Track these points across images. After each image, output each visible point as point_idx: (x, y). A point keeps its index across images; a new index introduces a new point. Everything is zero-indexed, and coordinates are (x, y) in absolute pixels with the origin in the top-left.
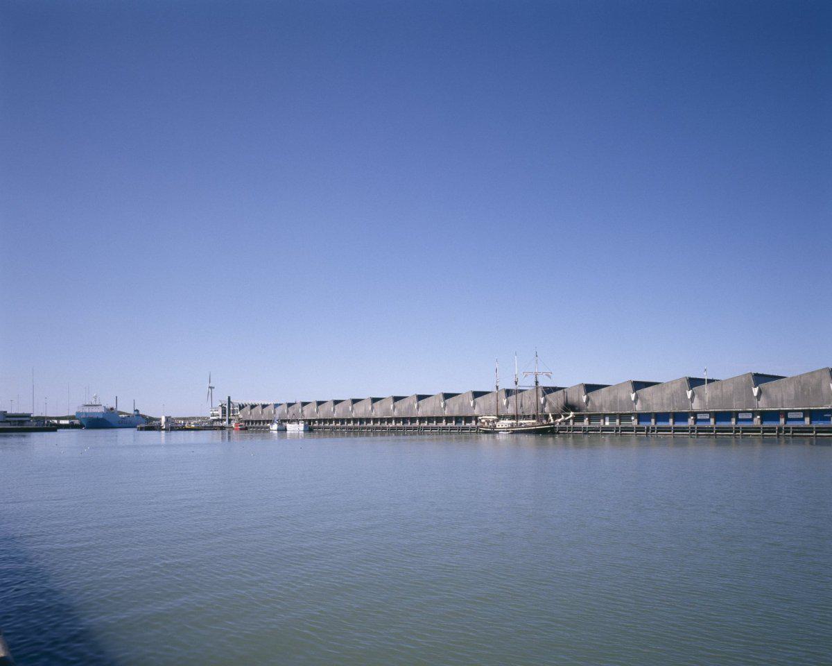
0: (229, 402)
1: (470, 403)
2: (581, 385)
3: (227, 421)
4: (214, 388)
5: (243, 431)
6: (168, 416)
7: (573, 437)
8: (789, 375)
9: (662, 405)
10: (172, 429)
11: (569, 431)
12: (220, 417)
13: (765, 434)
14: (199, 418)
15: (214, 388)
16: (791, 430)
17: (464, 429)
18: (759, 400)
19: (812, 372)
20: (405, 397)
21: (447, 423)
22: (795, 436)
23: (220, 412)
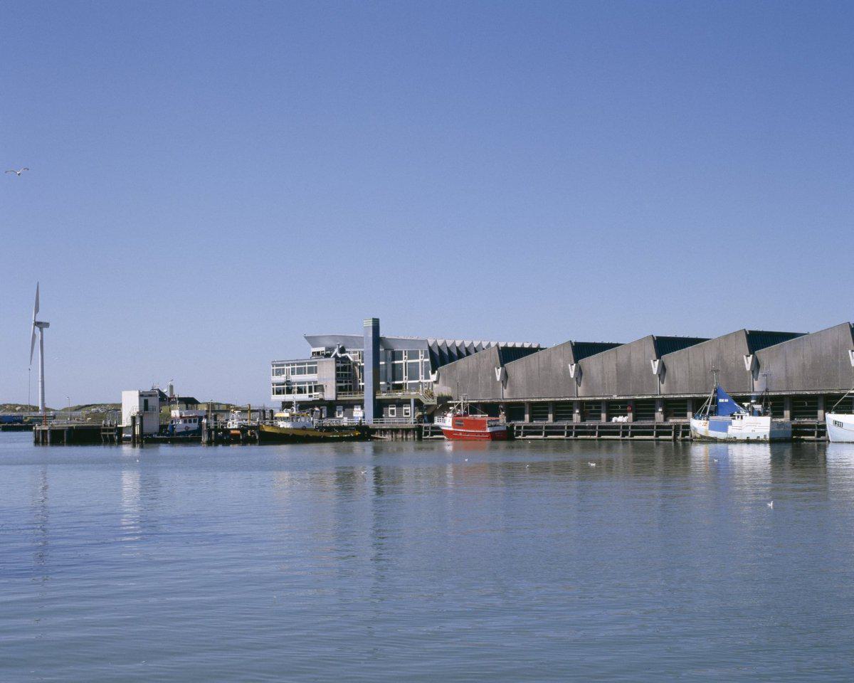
0: (377, 340)
1: (566, 372)
2: (736, 334)
3: (369, 405)
4: (47, 325)
5: (502, 444)
6: (148, 389)
7: (633, 444)
8: (713, 337)
9: (788, 379)
10: (167, 435)
11: (625, 434)
12: (330, 394)
13: (661, 437)
14: (95, 406)
15: (47, 325)
16: (205, 438)
17: (605, 430)
18: (579, 384)
19: (728, 335)
20: (618, 345)
21: (667, 415)
22: (549, 439)
23: (327, 374)
